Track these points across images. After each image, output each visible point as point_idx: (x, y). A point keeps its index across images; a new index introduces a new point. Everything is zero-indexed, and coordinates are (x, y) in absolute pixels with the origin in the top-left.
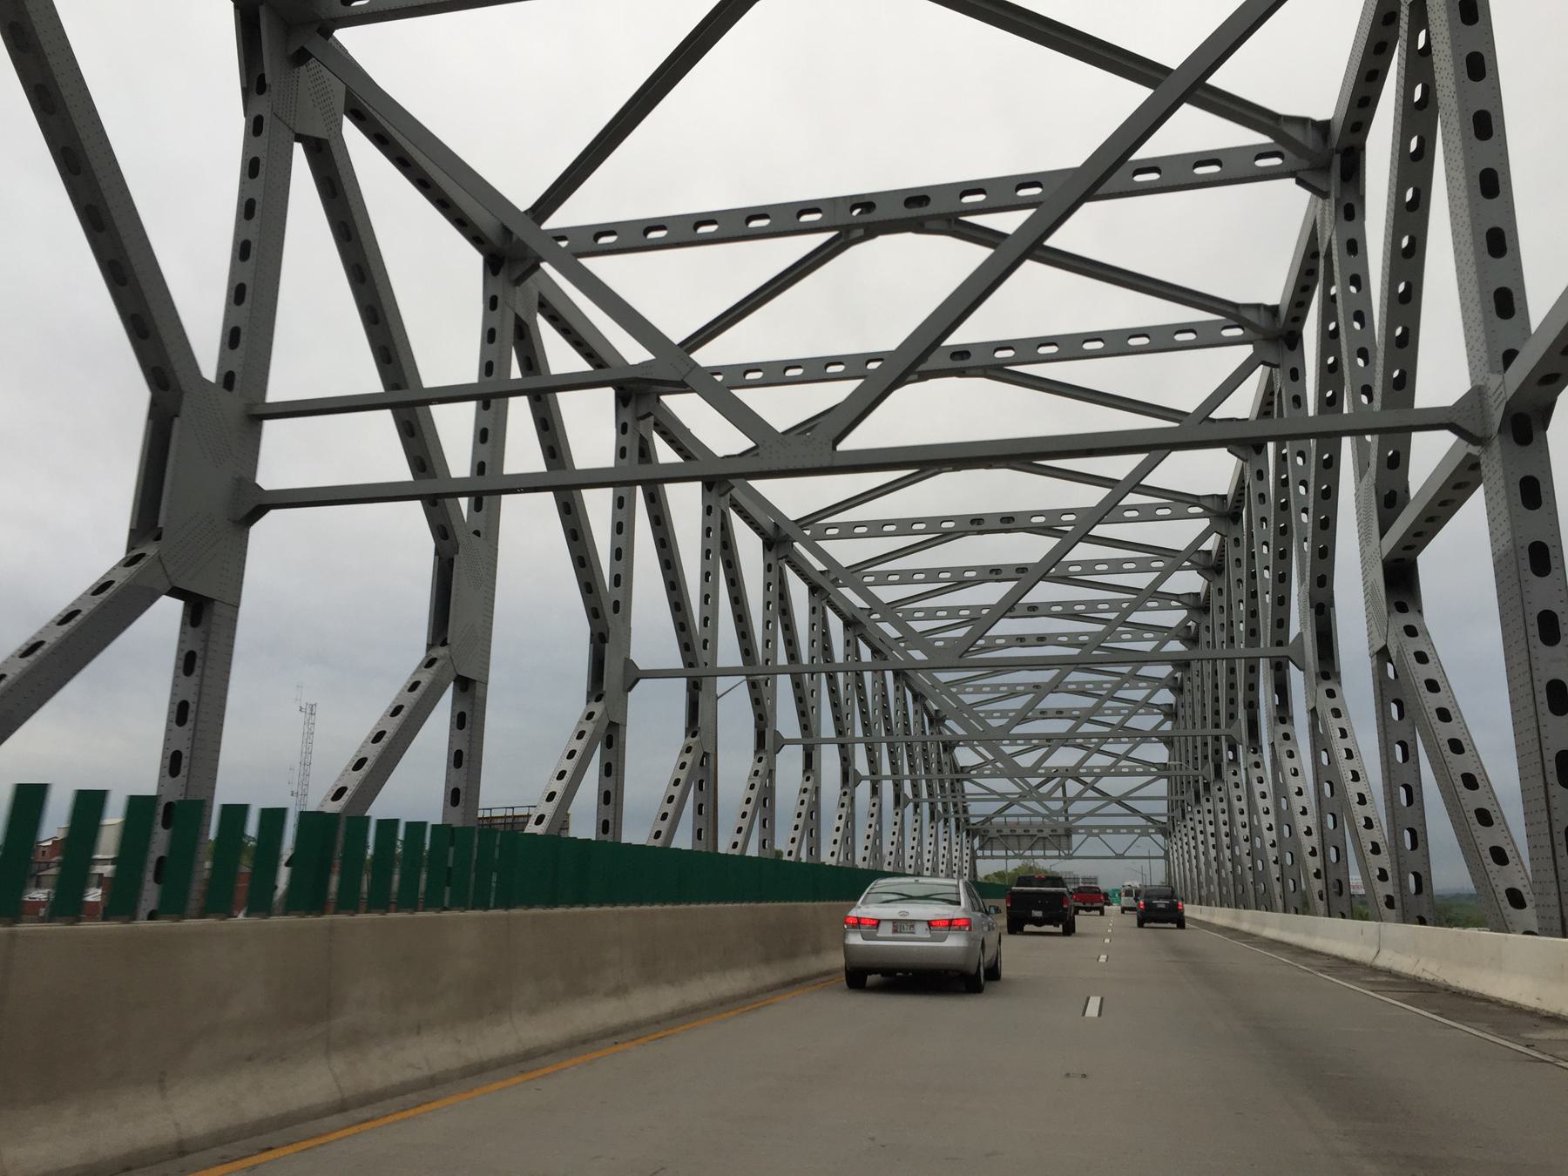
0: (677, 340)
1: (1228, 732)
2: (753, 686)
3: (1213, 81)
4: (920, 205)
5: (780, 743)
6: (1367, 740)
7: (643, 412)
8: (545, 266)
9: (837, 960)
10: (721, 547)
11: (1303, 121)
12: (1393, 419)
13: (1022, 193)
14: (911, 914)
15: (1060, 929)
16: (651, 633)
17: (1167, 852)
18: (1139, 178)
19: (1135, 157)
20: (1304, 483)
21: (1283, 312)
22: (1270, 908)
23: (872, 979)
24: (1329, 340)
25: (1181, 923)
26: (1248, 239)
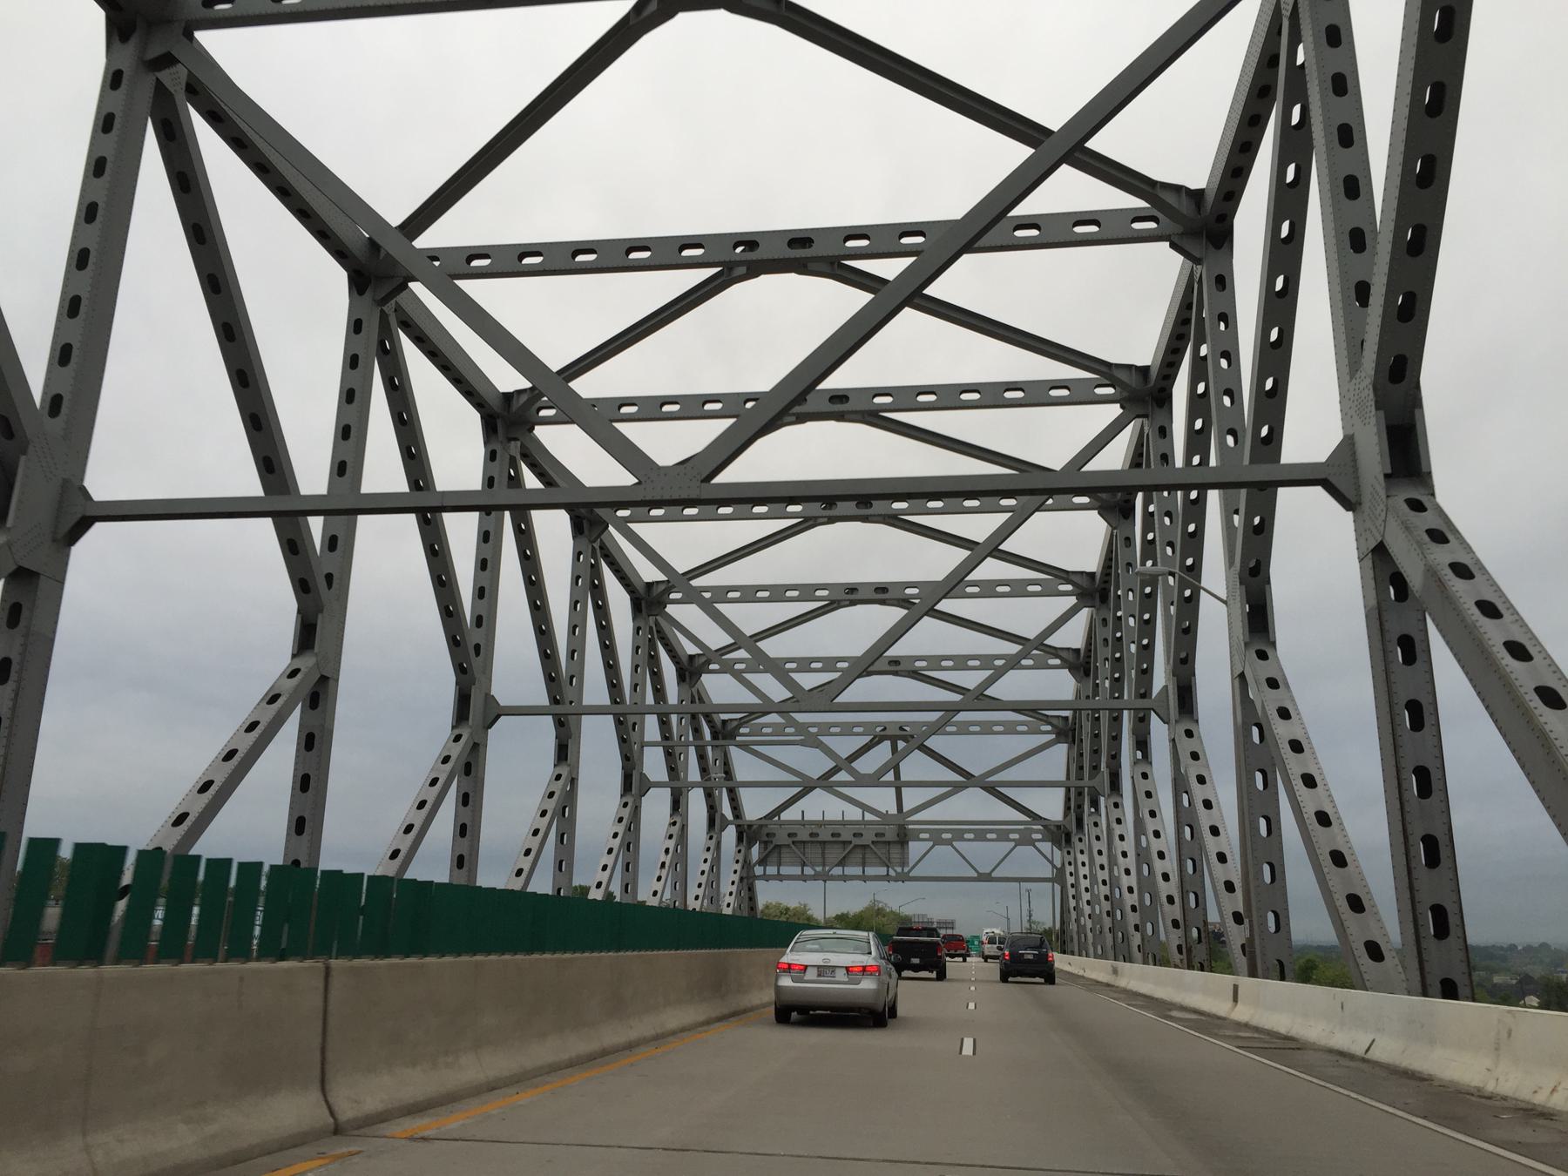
0: (555, 367)
1: (1091, 783)
2: (619, 723)
3: (1090, 144)
4: (804, 247)
5: (646, 785)
6: (1225, 791)
7: (154, 51)
8: (417, 287)
9: (768, 996)
10: (588, 588)
11: (1178, 189)
12: (1262, 473)
13: (905, 240)
14: (832, 961)
15: (934, 975)
16: (515, 667)
17: (1061, 871)
18: (1019, 233)
19: (1013, 213)
20: (1171, 544)
21: (1154, 373)
22: (1128, 958)
23: (794, 1015)
24: (1198, 404)
25: (1049, 977)
26: (1120, 300)
